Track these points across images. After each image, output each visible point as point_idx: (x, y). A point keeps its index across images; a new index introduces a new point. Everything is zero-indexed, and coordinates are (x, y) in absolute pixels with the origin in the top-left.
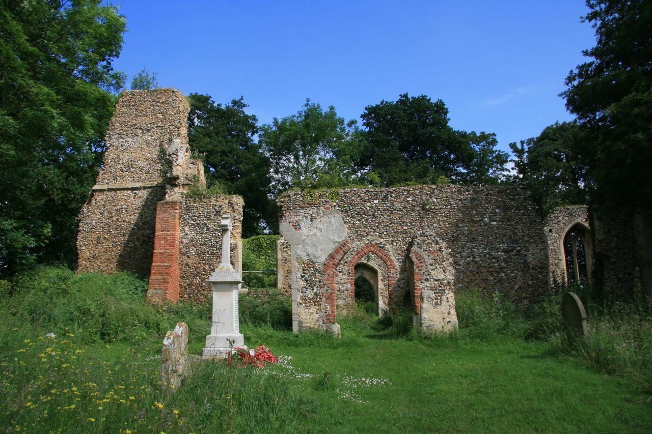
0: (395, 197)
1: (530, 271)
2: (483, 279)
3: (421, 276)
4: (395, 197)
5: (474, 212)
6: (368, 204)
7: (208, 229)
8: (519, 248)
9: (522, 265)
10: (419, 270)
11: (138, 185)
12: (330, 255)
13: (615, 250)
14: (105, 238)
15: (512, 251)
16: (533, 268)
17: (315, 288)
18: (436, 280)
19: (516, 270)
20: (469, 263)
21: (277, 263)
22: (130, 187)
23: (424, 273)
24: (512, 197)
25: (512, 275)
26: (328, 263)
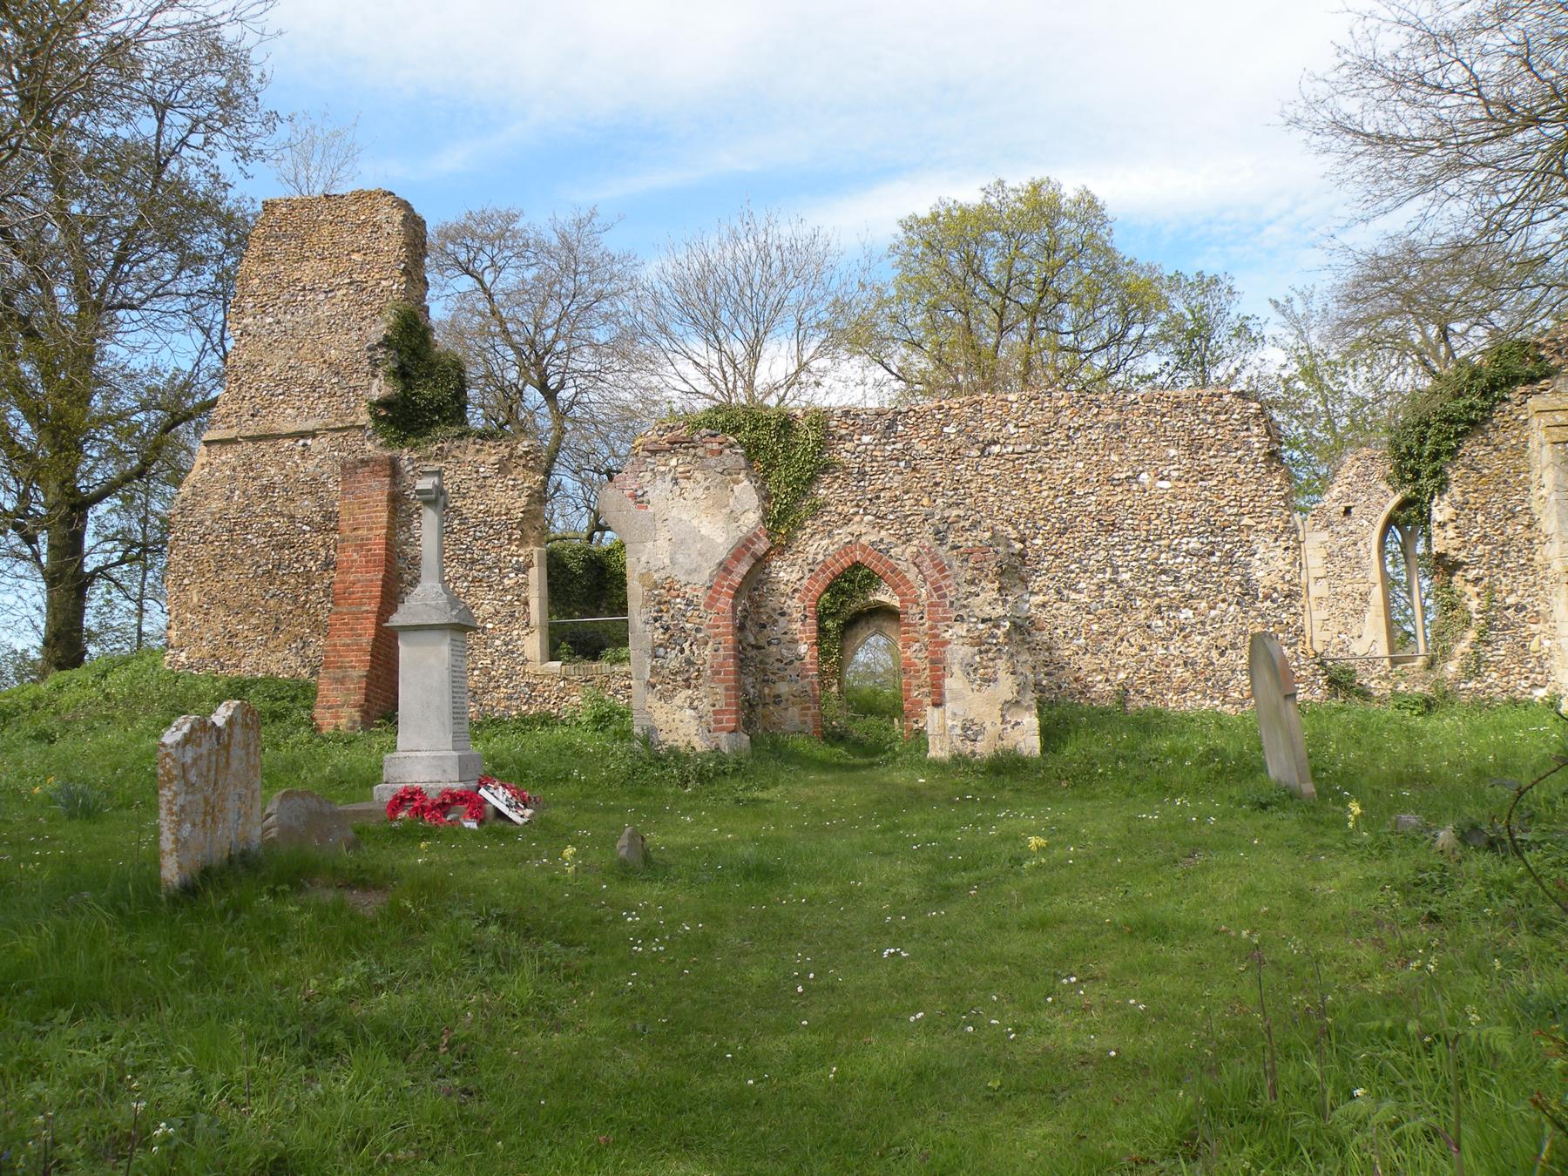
0: (916, 426)
1: (1258, 605)
2: (1139, 626)
3: (945, 612)
4: (916, 426)
5: (1114, 458)
6: (849, 446)
7: (464, 521)
8: (1228, 546)
9: (1238, 589)
10: (940, 597)
11: (310, 425)
12: (720, 564)
13: (1481, 547)
14: (234, 556)
15: (1213, 554)
16: (1267, 597)
17: (686, 646)
18: (984, 621)
19: (1224, 601)
20: (1101, 587)
21: (441, 541)
22: (292, 430)
23: (952, 603)
24: (1209, 418)
25: (1213, 613)
26: (717, 584)
